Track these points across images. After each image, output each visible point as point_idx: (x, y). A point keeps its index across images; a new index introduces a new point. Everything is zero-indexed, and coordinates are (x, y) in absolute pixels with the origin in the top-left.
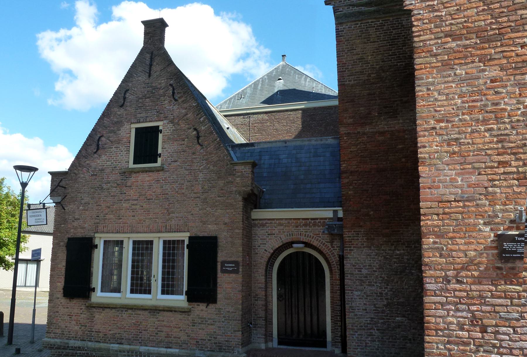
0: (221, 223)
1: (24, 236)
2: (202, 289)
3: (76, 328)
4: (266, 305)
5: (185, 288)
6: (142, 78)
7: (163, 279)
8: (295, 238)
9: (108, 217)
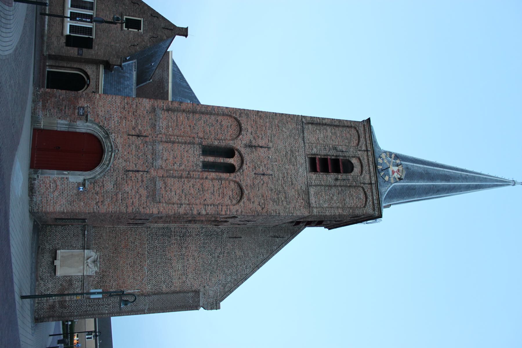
0: (97, 51)
2: (70, 41)
4: (64, 67)
5: (72, 34)
6: (163, 25)
7: (76, 26)
8: (91, 80)
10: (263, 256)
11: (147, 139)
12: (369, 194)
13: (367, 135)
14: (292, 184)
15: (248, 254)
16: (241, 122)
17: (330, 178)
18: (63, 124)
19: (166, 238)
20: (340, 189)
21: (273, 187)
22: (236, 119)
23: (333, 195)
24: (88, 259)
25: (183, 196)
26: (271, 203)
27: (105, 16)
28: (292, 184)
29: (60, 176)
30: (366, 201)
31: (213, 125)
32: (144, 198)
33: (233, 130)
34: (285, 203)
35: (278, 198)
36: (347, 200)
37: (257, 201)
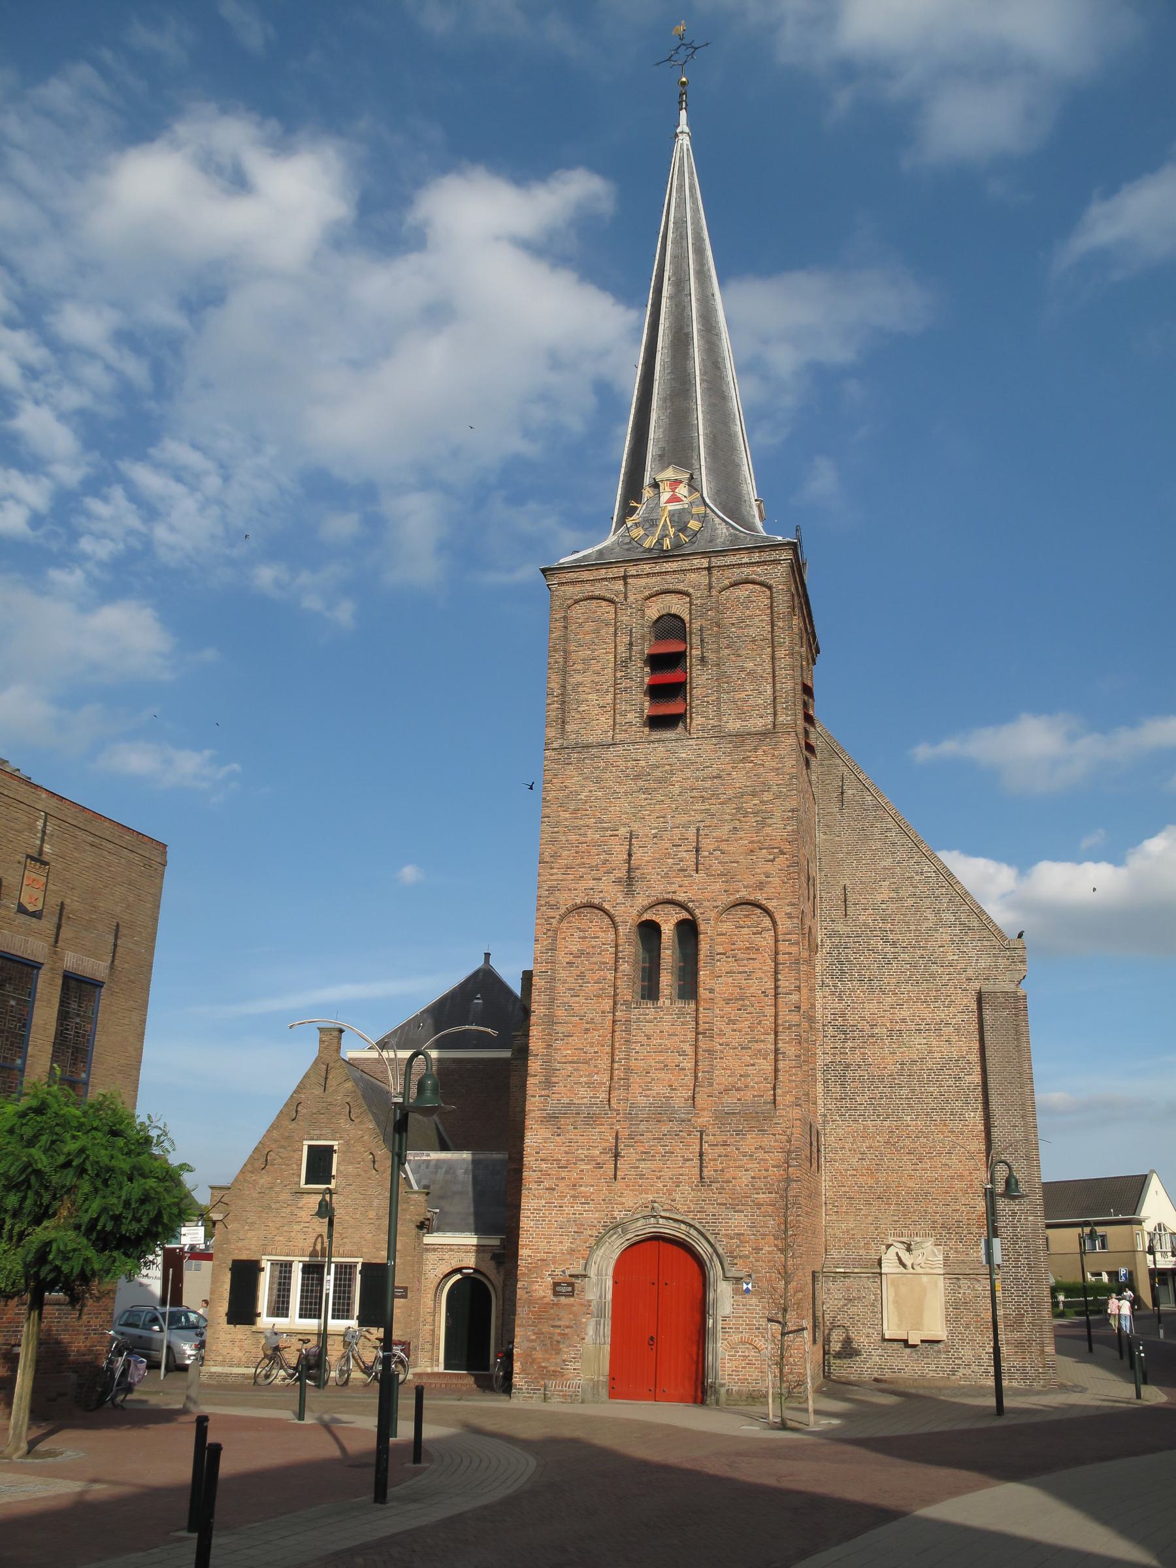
1: (378, 1249)
3: (240, 1354)
5: (356, 1312)
6: (318, 1091)
9: (277, 1238)
10: (889, 830)
11: (624, 1133)
12: (737, 574)
13: (586, 575)
14: (718, 777)
15: (885, 868)
16: (570, 903)
17: (700, 679)
18: (597, 1331)
19: (849, 1074)
20: (727, 651)
21: (727, 827)
22: (562, 918)
23: (743, 669)
24: (904, 1266)
25: (756, 1046)
26: (768, 830)
27: (305, 1233)
28: (718, 777)
29: (720, 1335)
30: (754, 582)
31: (582, 976)
32: (767, 1141)
33: (596, 925)
34: (767, 796)
35: (756, 813)
36: (752, 632)
37: (762, 867)
